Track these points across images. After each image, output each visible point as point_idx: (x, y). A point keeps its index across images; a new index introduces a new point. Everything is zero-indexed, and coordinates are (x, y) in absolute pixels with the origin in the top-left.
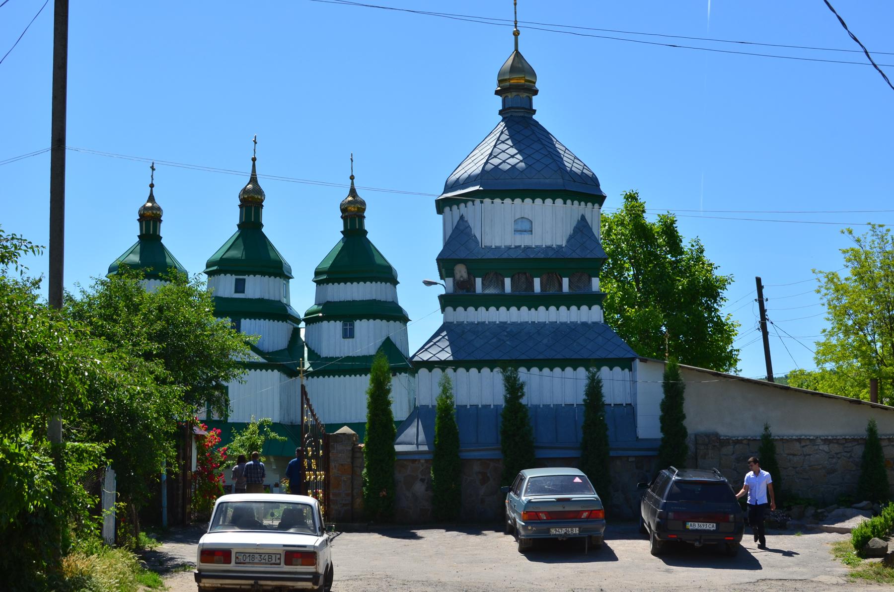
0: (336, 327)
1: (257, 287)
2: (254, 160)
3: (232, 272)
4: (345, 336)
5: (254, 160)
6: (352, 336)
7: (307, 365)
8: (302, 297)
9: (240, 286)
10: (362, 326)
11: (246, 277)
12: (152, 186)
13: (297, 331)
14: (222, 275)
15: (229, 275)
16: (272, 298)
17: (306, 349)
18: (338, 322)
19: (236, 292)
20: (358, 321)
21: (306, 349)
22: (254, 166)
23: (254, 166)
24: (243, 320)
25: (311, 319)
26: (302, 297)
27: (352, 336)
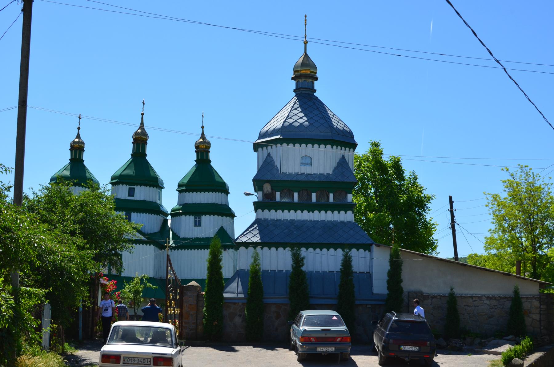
0: (189, 220)
1: (142, 193)
2: (142, 114)
3: (127, 184)
4: (195, 225)
5: (142, 114)
6: (199, 225)
7: (171, 242)
8: (170, 200)
9: (131, 192)
10: (206, 219)
11: (135, 187)
12: (79, 128)
13: (166, 221)
14: (121, 185)
15: (125, 185)
16: (151, 200)
17: (171, 232)
19: (129, 196)
20: (204, 216)
21: (171, 232)
22: (142, 118)
23: (142, 118)
24: (132, 214)
25: (174, 214)
26: (170, 200)
27: (199, 225)
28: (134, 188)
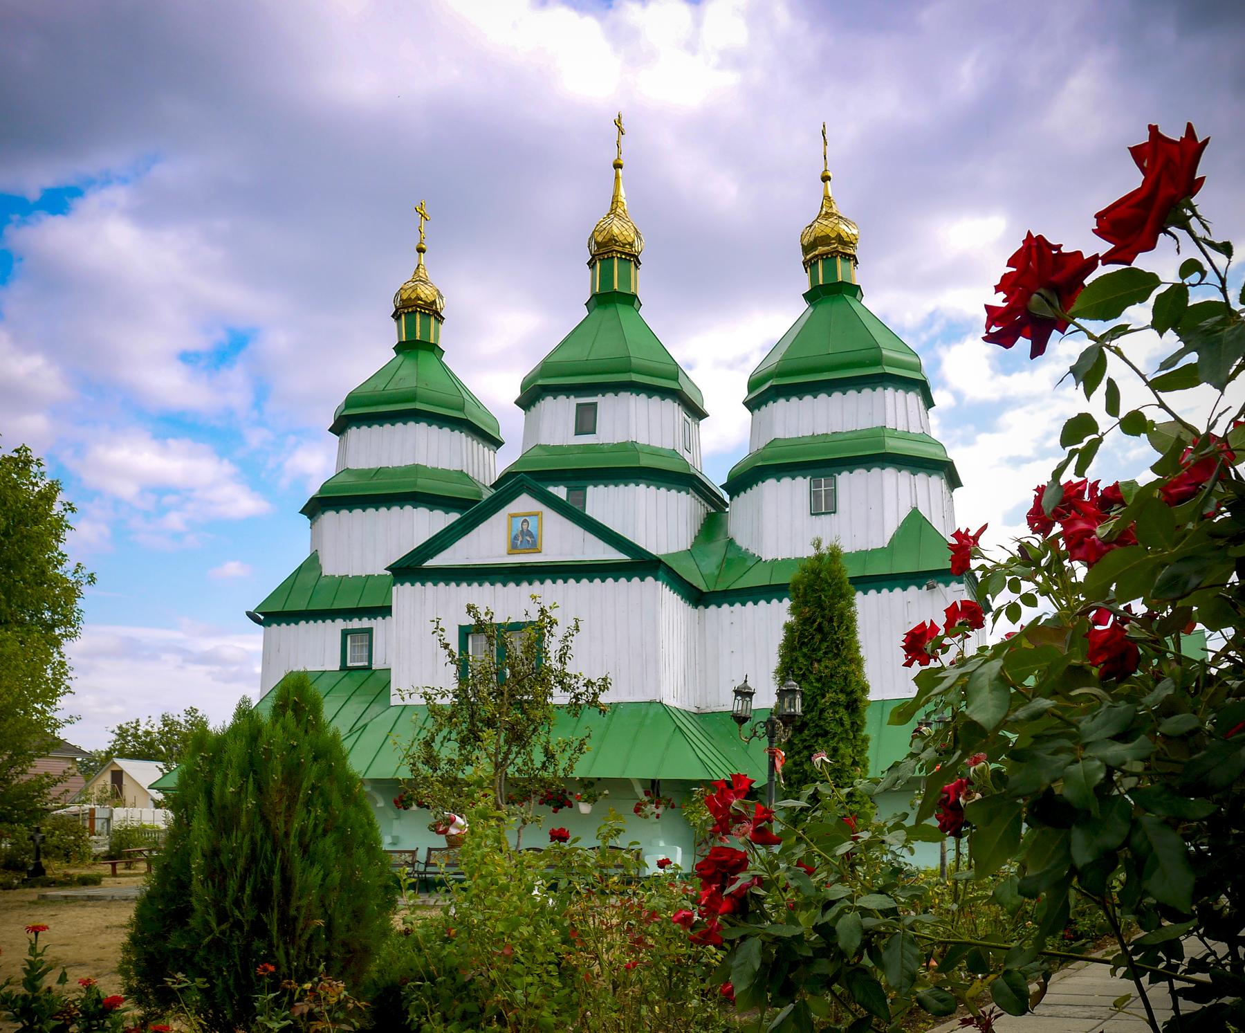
1: (631, 422)
10: (849, 484)
11: (598, 399)
15: (562, 398)
18: (799, 479)
20: (845, 474)
28: (594, 406)
